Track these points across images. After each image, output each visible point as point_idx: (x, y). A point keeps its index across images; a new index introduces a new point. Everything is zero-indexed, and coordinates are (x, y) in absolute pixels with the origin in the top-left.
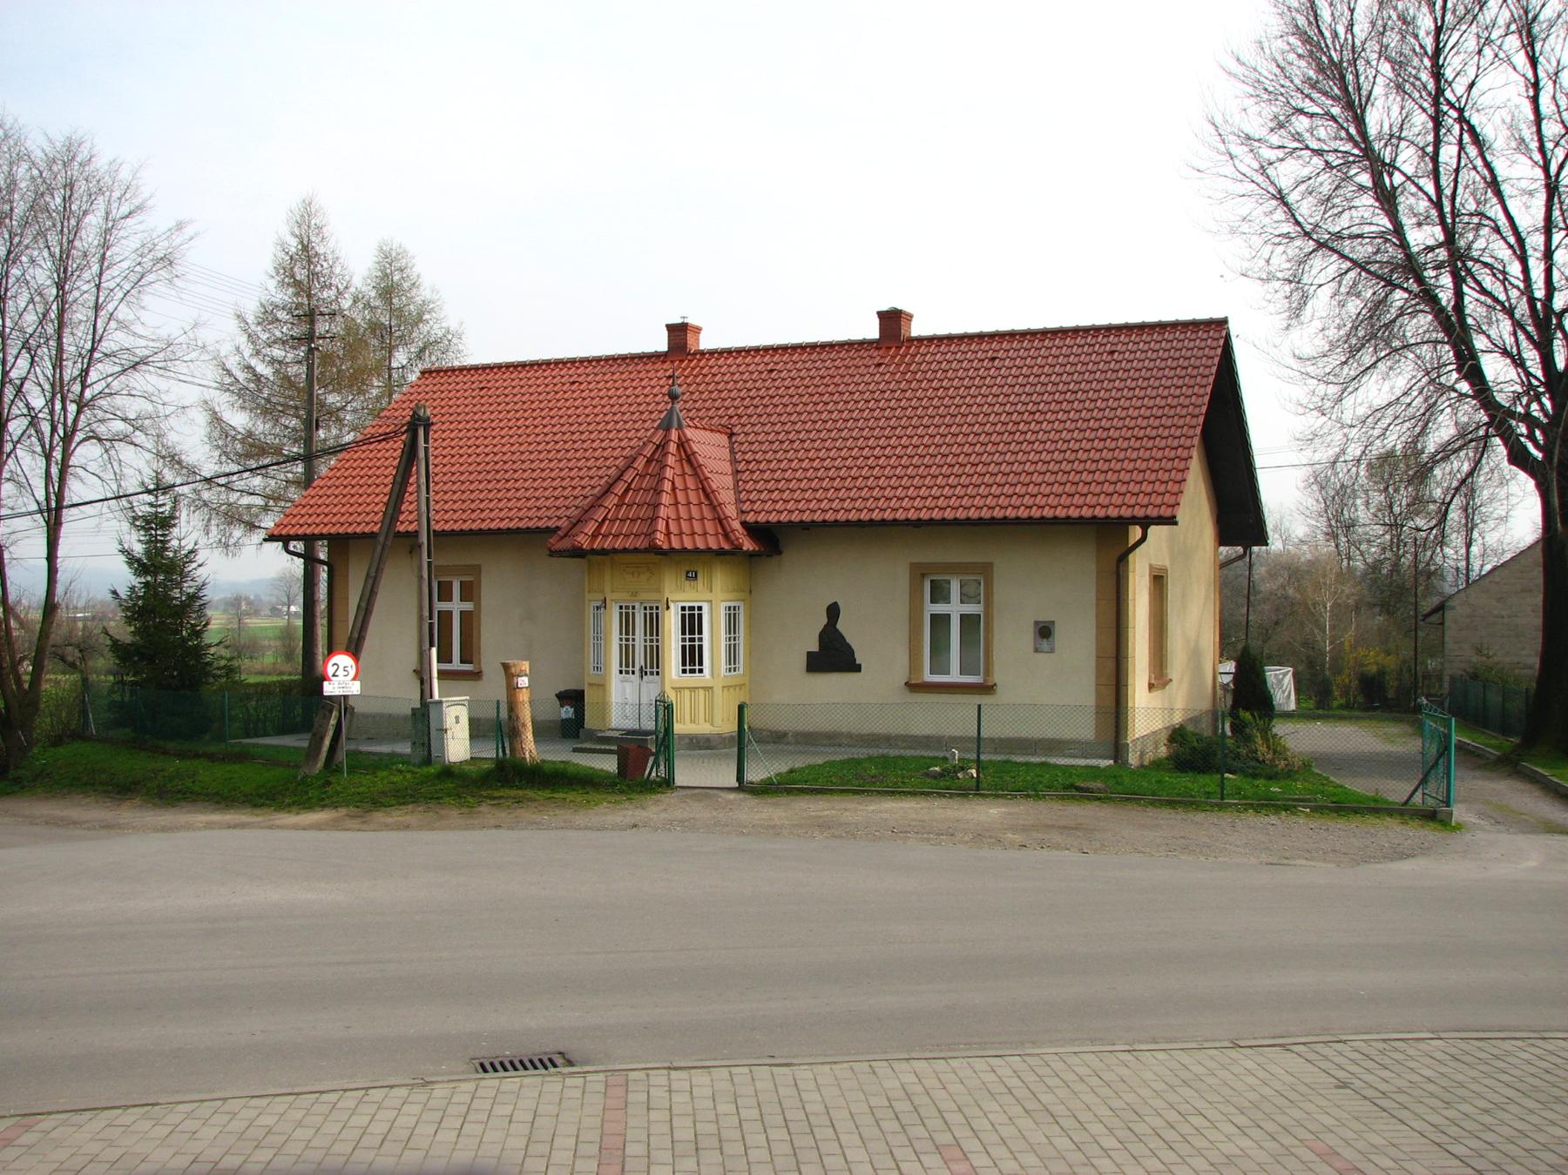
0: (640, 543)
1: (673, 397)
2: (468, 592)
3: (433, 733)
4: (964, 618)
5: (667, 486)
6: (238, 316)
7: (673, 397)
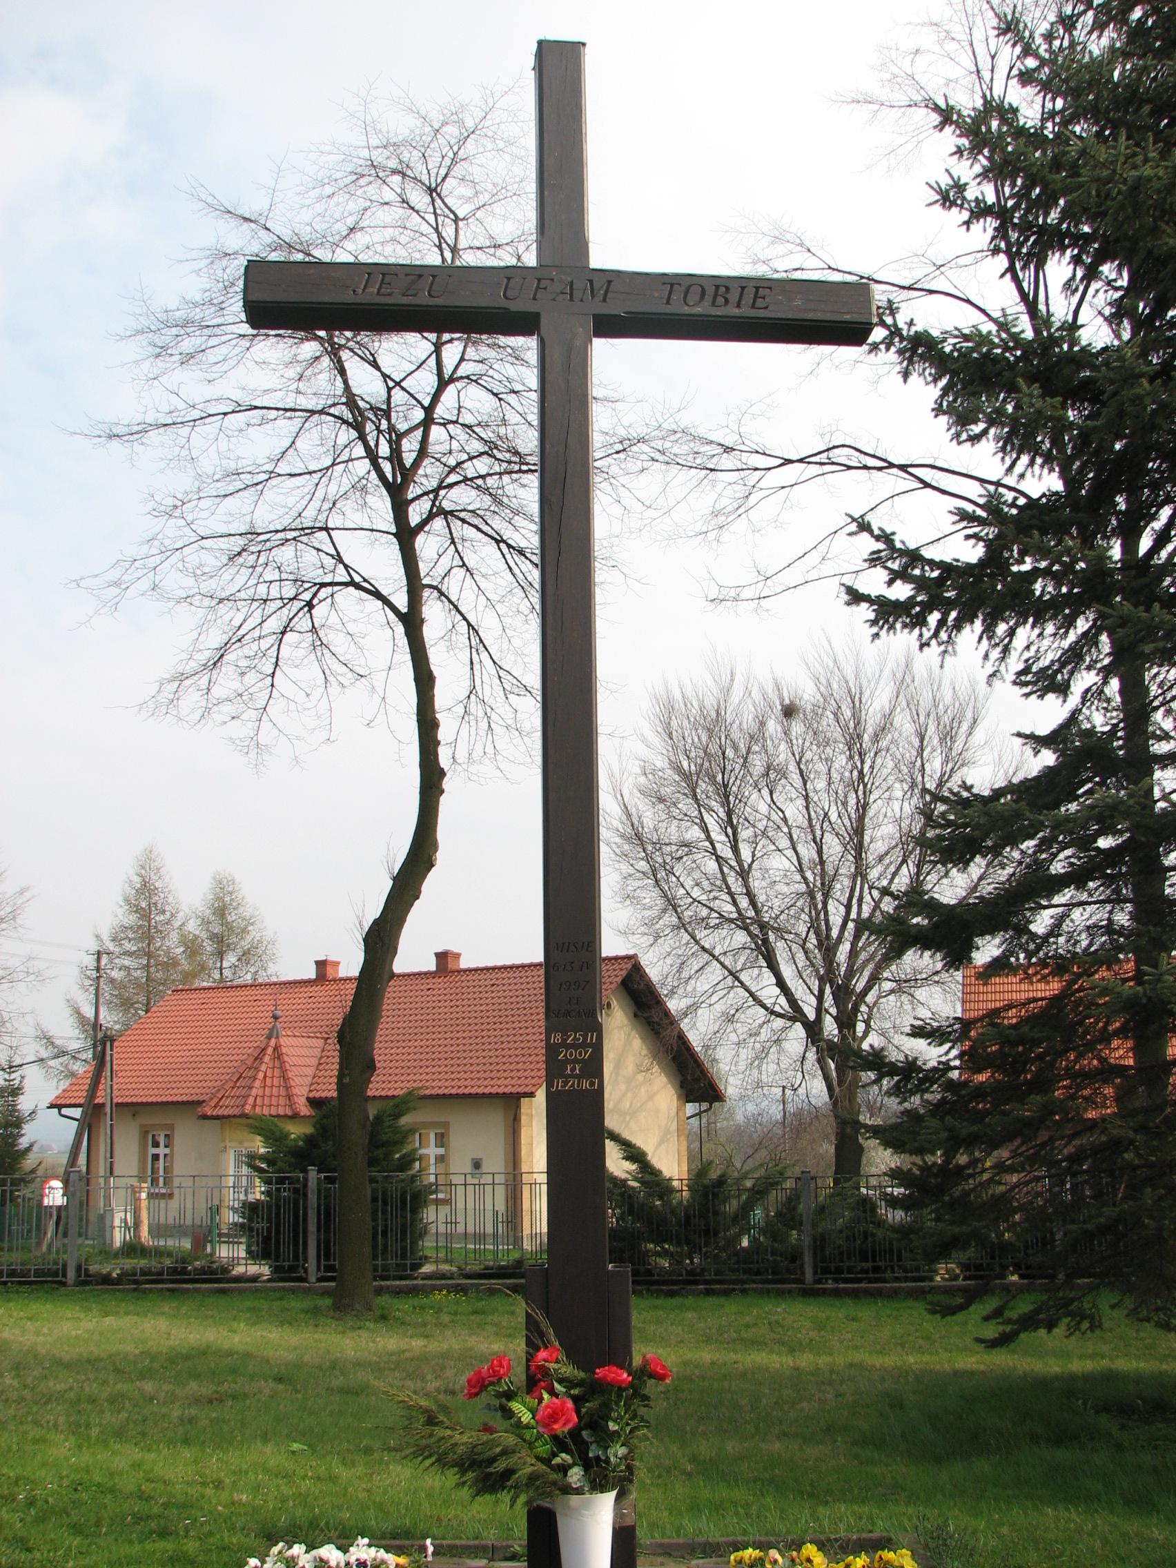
0: (237, 1111)
1: (276, 1018)
2: (441, 1140)
3: (108, 1229)
4: (165, 1155)
5: (261, 1075)
6: (97, 936)
7: (276, 1018)
